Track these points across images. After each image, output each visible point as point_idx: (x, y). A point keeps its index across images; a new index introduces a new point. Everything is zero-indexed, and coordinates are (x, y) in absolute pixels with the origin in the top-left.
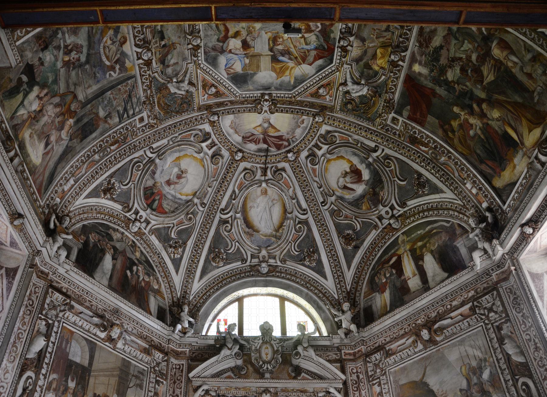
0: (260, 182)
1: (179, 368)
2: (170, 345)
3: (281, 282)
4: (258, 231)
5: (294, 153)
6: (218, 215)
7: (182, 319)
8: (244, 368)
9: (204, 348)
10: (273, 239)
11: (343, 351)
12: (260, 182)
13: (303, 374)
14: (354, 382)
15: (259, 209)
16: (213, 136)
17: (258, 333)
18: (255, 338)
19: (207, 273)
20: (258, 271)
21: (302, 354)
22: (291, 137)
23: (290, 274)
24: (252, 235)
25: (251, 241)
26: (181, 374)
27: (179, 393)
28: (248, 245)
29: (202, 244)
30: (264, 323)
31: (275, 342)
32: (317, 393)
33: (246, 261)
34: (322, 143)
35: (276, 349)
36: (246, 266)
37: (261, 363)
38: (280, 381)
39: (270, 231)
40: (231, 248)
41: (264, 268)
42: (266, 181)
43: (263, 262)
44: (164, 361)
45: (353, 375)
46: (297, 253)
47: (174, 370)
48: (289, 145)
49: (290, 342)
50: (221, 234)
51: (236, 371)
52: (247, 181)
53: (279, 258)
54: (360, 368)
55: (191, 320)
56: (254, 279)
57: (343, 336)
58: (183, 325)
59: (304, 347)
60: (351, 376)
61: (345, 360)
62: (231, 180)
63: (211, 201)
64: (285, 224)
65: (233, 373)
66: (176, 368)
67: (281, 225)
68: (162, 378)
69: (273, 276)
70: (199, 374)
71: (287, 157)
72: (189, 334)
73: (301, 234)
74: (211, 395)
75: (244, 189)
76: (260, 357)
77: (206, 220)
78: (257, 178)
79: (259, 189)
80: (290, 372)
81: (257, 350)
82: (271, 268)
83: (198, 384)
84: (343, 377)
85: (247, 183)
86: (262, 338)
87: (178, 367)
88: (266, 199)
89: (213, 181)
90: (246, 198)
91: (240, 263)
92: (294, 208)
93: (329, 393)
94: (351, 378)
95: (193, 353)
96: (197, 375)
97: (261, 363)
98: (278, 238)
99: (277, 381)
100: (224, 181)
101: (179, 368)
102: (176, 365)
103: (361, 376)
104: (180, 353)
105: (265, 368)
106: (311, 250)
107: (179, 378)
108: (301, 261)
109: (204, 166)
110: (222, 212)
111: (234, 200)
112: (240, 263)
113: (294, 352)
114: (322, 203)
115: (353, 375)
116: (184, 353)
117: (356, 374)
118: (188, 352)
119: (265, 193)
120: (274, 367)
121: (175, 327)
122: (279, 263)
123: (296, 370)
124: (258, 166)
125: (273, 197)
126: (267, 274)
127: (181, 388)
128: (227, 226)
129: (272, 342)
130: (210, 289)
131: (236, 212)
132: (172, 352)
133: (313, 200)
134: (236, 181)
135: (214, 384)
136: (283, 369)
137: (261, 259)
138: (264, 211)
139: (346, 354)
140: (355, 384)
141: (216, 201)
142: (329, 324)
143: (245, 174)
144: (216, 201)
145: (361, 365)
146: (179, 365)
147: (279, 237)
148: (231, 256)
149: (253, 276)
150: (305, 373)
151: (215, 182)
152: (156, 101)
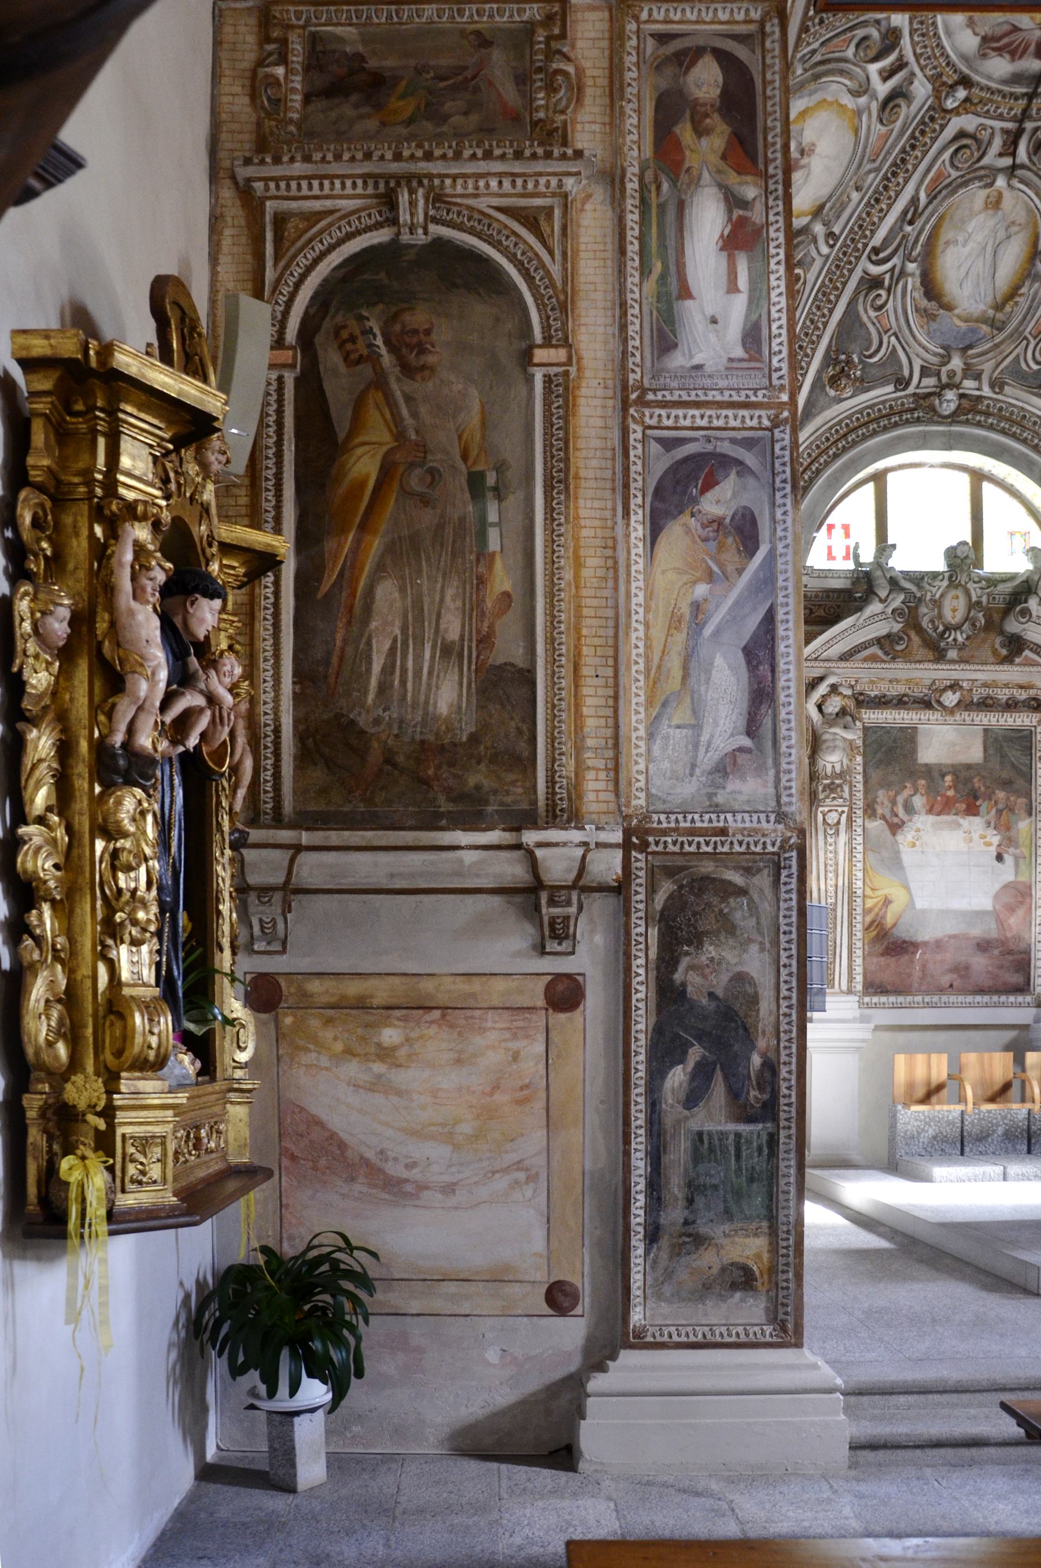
0: (994, 172)
3: (985, 440)
4: (949, 308)
6: (864, 264)
8: (901, 639)
9: (816, 596)
10: (985, 329)
12: (994, 172)
13: (1027, 653)
15: (968, 249)
16: (906, 41)
17: (939, 565)
18: (935, 575)
19: (815, 416)
21: (1034, 614)
23: (1008, 420)
24: (931, 317)
25: (928, 334)
28: (920, 344)
29: (813, 342)
33: (908, 384)
35: (974, 599)
36: (906, 396)
38: (985, 668)
39: (983, 307)
40: (877, 351)
41: (950, 401)
42: (1011, 171)
43: (949, 386)
50: (858, 316)
51: (887, 643)
52: (957, 169)
56: (921, 428)
62: (916, 167)
63: (852, 228)
64: (1023, 290)
67: (1013, 293)
69: (967, 422)
75: (944, 192)
76: (940, 616)
77: (831, 280)
78: (985, 161)
79: (984, 193)
80: (997, 646)
82: (965, 403)
83: (817, 673)
85: (954, 174)
86: (951, 577)
88: (991, 223)
89: (870, 172)
90: (941, 218)
91: (890, 388)
98: (997, 326)
99: (980, 667)
100: (900, 167)
109: (856, 131)
110: (874, 258)
111: (911, 223)
112: (890, 388)
119: (995, 204)
122: (986, 391)
124: (998, 124)
125: (1011, 218)
126: (953, 418)
128: (879, 295)
130: (820, 455)
131: (908, 258)
134: (928, 170)
136: (984, 641)
137: (944, 379)
138: (978, 256)
141: (864, 227)
143: (957, 151)
144: (864, 227)
147: (999, 324)
148: (873, 371)
149: (918, 421)
150: (1031, 650)
151: (872, 176)
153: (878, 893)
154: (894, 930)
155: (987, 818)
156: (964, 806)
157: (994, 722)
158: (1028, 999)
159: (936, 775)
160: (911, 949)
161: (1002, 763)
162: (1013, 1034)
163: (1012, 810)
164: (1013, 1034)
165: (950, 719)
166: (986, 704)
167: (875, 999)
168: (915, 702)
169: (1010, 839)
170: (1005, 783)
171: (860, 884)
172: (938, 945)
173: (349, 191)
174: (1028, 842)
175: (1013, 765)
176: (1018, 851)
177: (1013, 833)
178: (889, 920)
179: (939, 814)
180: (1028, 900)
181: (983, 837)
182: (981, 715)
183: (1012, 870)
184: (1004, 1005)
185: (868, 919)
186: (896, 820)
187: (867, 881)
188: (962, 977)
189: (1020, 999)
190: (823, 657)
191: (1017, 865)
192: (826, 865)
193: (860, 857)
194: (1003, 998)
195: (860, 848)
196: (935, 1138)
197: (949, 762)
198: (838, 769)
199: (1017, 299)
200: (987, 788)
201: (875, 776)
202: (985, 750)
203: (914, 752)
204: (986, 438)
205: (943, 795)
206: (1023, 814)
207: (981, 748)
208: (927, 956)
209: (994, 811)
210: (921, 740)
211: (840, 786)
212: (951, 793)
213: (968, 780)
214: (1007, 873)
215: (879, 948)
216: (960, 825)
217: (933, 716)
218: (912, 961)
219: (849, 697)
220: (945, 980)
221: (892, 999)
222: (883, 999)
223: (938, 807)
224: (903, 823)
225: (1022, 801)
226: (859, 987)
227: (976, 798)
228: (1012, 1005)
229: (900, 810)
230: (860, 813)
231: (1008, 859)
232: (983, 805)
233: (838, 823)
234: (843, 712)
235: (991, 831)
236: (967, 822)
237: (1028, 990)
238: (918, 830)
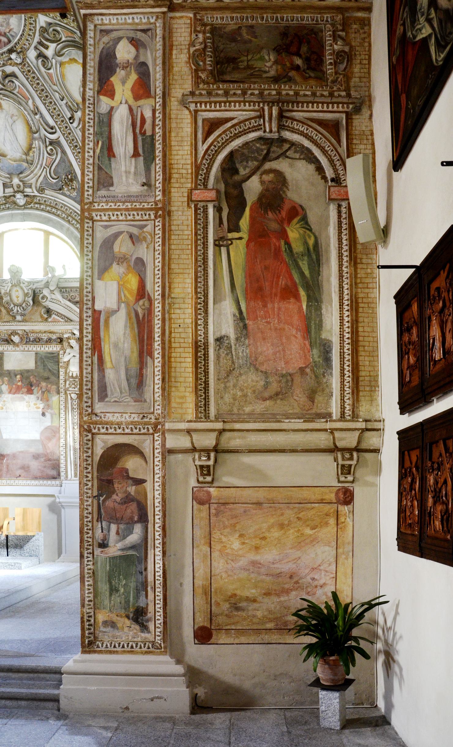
3: (41, 216)
5: (18, 53)
10: (25, 165)
13: (53, 316)
20: (15, 203)
21: (49, 298)
22: (8, 30)
30: (11, 266)
34: (47, 40)
35: (26, 291)
38: (26, 324)
39: (20, 155)
43: (18, 192)
46: (54, 181)
48: (10, 41)
49: (39, 284)
53: (36, 187)
56: (10, 212)
59: (51, 291)
64: (34, 146)
67: (30, 148)
71: (11, 59)
73: (54, 157)
80: (42, 313)
81: (7, 293)
92: (40, 126)
97: (12, 306)
106: (69, 176)
108: (60, 189)
114: (70, 119)
122: (36, 193)
126: (25, 207)
129: (22, 285)
133: (59, 115)
137: (16, 189)
147: (31, 162)
155: (38, 395)
156: (26, 390)
157: (39, 349)
159: (12, 375)
161: (44, 369)
163: (49, 391)
165: (17, 349)
166: (38, 341)
169: (48, 405)
172: (14, 456)
173: (218, 108)
175: (50, 370)
176: (52, 411)
177: (50, 403)
179: (14, 394)
180: (57, 435)
181: (35, 404)
183: (50, 420)
191: (52, 417)
197: (19, 369)
199: (33, 150)
200: (37, 381)
202: (36, 363)
204: (41, 215)
205: (16, 385)
206: (54, 393)
209: (40, 392)
210: (5, 358)
212: (20, 384)
213: (28, 378)
214: (47, 422)
216: (24, 399)
217: (10, 347)
220: (18, 472)
223: (13, 391)
225: (54, 387)
227: (31, 386)
231: (48, 415)
232: (35, 390)
235: (39, 402)
236: (28, 397)
238: (4, 401)
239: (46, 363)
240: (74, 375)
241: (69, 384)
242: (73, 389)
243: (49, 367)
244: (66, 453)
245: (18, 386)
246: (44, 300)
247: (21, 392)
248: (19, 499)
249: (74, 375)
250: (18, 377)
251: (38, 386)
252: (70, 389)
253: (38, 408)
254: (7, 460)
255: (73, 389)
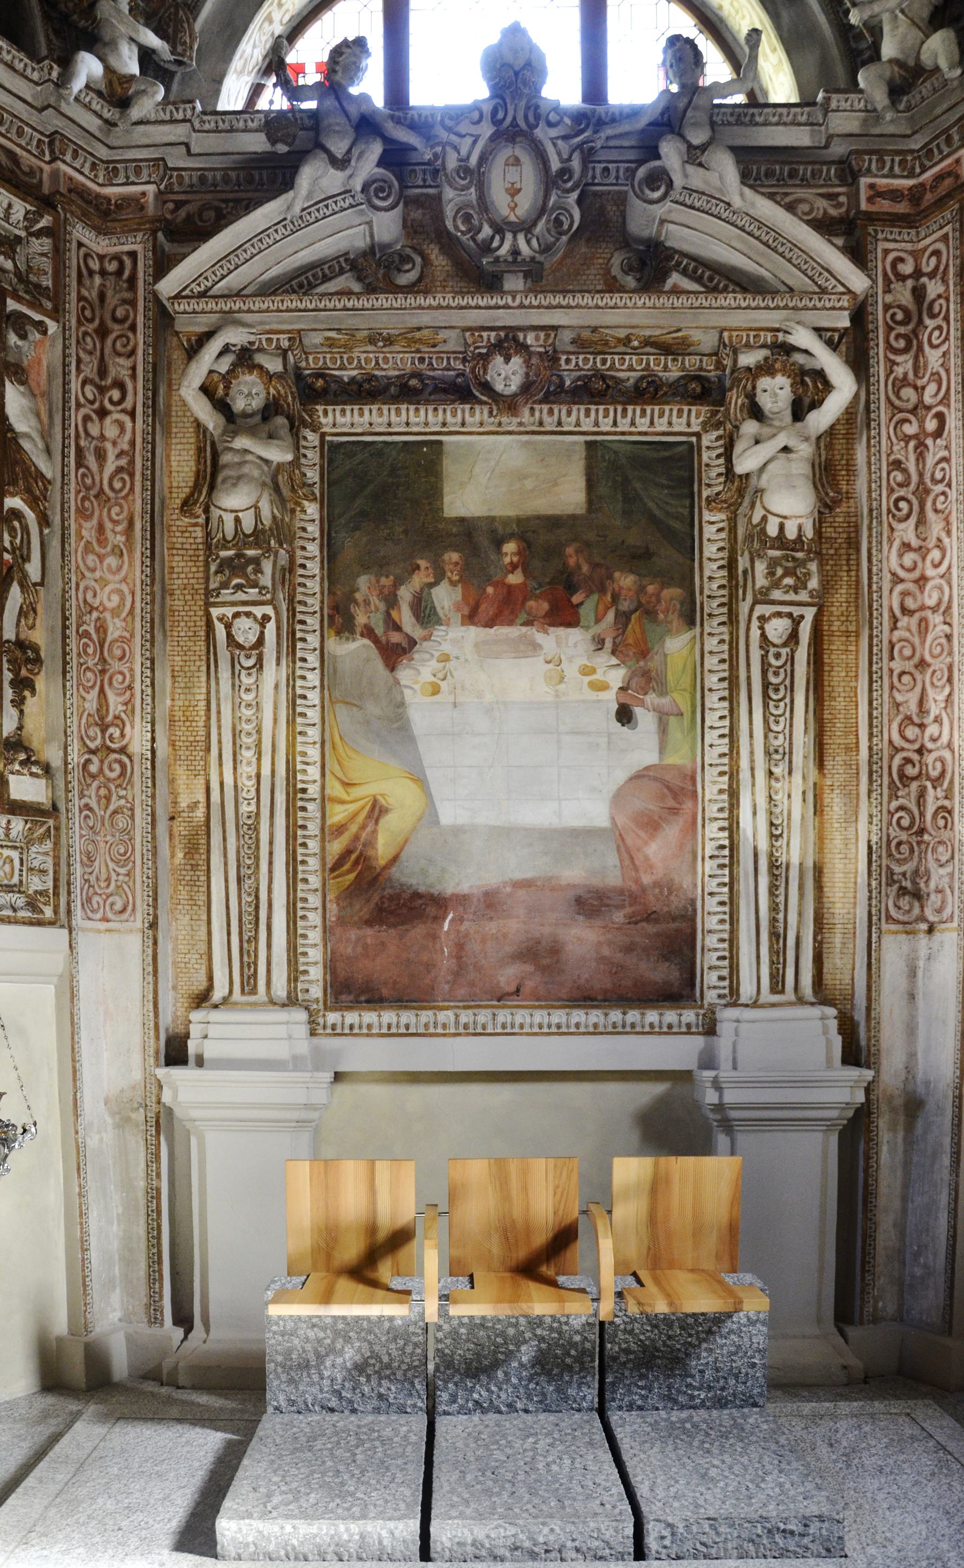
1: (119, 272)
2: (63, 167)
7: (107, 35)
8: (409, 259)
9: (226, 180)
11: (864, 181)
13: (675, 279)
14: (900, 316)
21: (678, 181)
26: (127, 295)
27: (125, 374)
31: (553, 133)
32: (735, 352)
35: (555, 165)
37: (487, 231)
38: (569, 300)
44: (39, 234)
45: (896, 286)
47: (97, 280)
54: (937, 253)
55: (152, 40)
57: (880, 97)
58: (113, 62)
59: (690, 147)
60: (887, 290)
61: (871, 218)
65: (359, 279)
66: (103, 273)
68: (35, 305)
70: (206, 284)
72: (144, 107)
74: (261, 367)
76: (484, 204)
80: (615, 271)
83: (201, 325)
84: (858, 281)
86: (494, 112)
87: (112, 267)
93: (789, 349)
94: (889, 298)
95: (179, 205)
96: (197, 289)
97: (487, 231)
99: (559, 299)
101: (119, 272)
102: (101, 258)
103: (933, 288)
104: (119, 207)
105: (504, 251)
107: (120, 313)
113: (642, 172)
115: (896, 286)
116: (135, 203)
117: (910, 283)
118: (151, 198)
120: (546, 249)
121: (66, 63)
123: (643, 263)
127: (133, 353)
129: (540, 132)
132: (74, 196)
135: (273, 321)
139: (876, 193)
140: (900, 323)
142: (811, 59)
145: (945, 238)
146: (117, 257)
150: (684, 273)
152: (196, 47)
153: (356, 792)
154: (394, 871)
155: (596, 629)
156: (545, 606)
158: (689, 1016)
159: (484, 542)
160: (432, 911)
161: (626, 514)
162: (659, 1088)
163: (650, 613)
164: (659, 1088)
165: (510, 422)
167: (352, 1017)
168: (436, 390)
170: (634, 557)
171: (314, 772)
174: (686, 680)
175: (653, 518)
176: (664, 701)
177: (654, 663)
178: (383, 849)
179: (490, 624)
180: (688, 805)
181: (587, 671)
182: (578, 411)
183: (653, 741)
184: (634, 1030)
185: (336, 847)
186: (395, 638)
187: (331, 764)
188: (544, 969)
189: (671, 1016)
190: (215, 291)
191: (663, 730)
192: (235, 734)
193: (313, 715)
194: (633, 1016)
195: (314, 697)
196: (360, 1368)
197: (511, 512)
198: (248, 524)
200: (595, 566)
201: (350, 548)
202: (591, 485)
203: (435, 493)
206: (675, 620)
207: (581, 483)
208: (466, 925)
209: (611, 616)
210: (449, 466)
211: (256, 561)
213: (554, 551)
215: (362, 909)
216: (536, 647)
217: (478, 416)
218: (434, 937)
219: (279, 376)
220: (508, 976)
221: (389, 1016)
222: (370, 1017)
223: (487, 609)
224: (413, 643)
225: (672, 593)
226: (316, 992)
227: (571, 588)
228: (652, 1031)
229: (406, 617)
230: (313, 622)
231: (645, 718)
233: (260, 642)
234: (271, 409)
235: (605, 659)
237: (692, 997)
238: (445, 658)
239: (638, 485)
240: (791, 533)
241: (771, 574)
242: (791, 597)
243: (651, 504)
244: (732, 885)
245: (510, 587)
246: (656, 195)
247: (523, 617)
248: (506, 1091)
249: (791, 533)
250: (510, 547)
251: (602, 590)
252: (777, 595)
253: (601, 687)
254: (459, 920)
255: (791, 597)
